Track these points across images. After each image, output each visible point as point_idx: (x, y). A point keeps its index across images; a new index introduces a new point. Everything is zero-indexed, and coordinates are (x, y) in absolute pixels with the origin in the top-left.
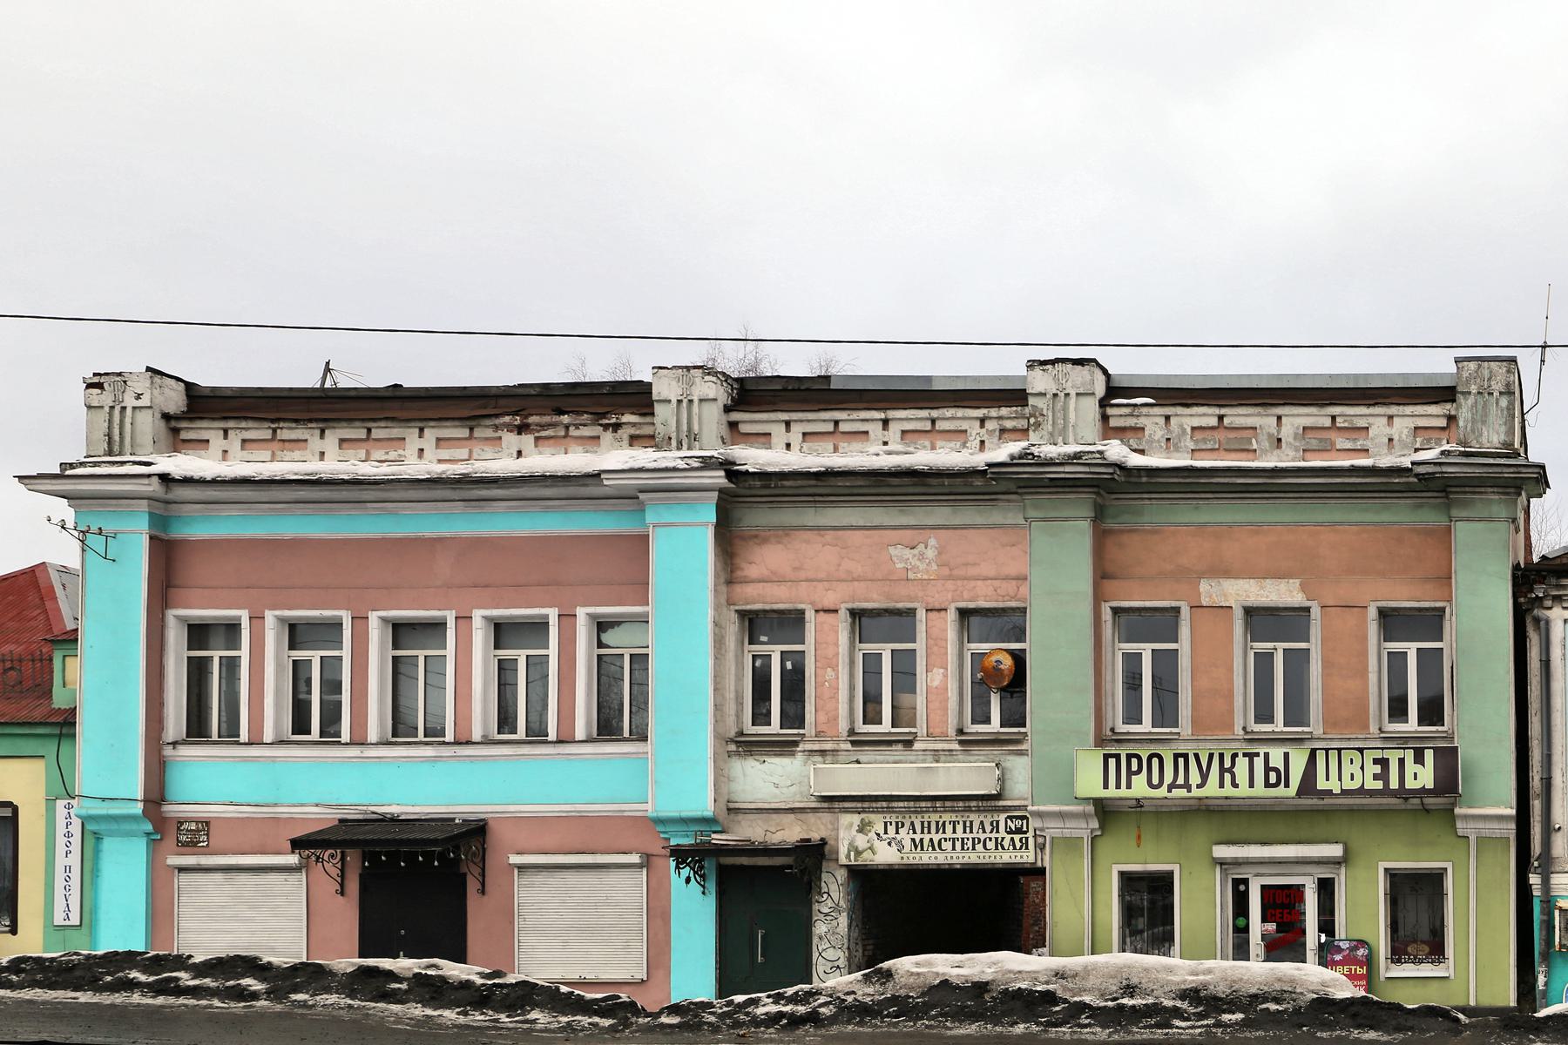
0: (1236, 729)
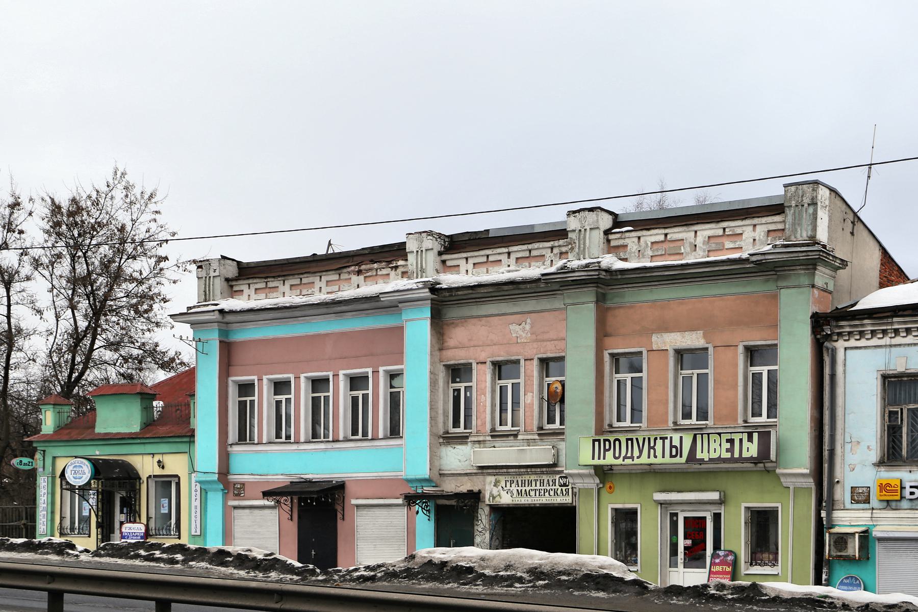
0: (669, 423)
